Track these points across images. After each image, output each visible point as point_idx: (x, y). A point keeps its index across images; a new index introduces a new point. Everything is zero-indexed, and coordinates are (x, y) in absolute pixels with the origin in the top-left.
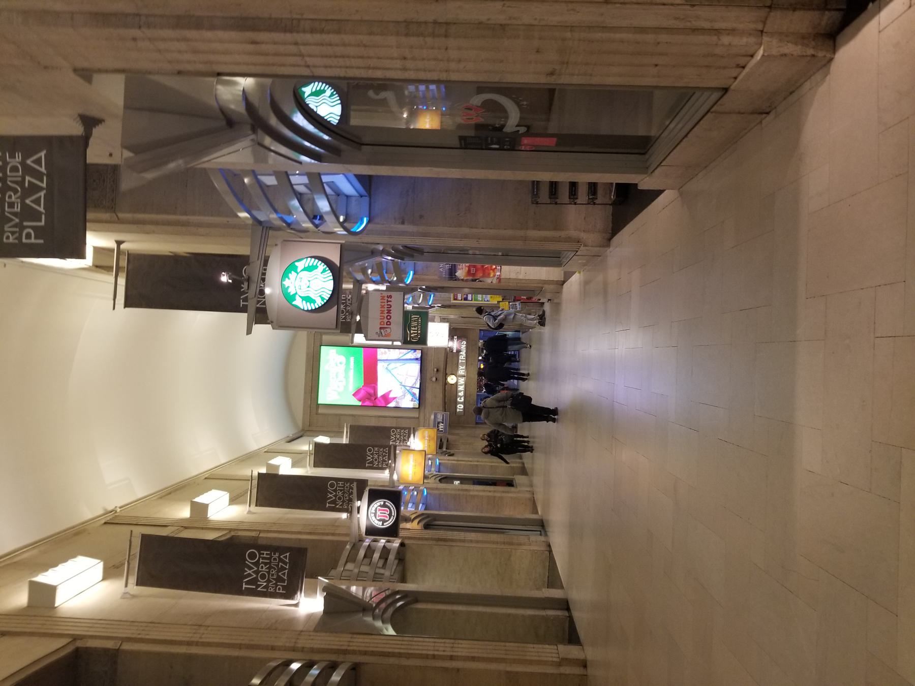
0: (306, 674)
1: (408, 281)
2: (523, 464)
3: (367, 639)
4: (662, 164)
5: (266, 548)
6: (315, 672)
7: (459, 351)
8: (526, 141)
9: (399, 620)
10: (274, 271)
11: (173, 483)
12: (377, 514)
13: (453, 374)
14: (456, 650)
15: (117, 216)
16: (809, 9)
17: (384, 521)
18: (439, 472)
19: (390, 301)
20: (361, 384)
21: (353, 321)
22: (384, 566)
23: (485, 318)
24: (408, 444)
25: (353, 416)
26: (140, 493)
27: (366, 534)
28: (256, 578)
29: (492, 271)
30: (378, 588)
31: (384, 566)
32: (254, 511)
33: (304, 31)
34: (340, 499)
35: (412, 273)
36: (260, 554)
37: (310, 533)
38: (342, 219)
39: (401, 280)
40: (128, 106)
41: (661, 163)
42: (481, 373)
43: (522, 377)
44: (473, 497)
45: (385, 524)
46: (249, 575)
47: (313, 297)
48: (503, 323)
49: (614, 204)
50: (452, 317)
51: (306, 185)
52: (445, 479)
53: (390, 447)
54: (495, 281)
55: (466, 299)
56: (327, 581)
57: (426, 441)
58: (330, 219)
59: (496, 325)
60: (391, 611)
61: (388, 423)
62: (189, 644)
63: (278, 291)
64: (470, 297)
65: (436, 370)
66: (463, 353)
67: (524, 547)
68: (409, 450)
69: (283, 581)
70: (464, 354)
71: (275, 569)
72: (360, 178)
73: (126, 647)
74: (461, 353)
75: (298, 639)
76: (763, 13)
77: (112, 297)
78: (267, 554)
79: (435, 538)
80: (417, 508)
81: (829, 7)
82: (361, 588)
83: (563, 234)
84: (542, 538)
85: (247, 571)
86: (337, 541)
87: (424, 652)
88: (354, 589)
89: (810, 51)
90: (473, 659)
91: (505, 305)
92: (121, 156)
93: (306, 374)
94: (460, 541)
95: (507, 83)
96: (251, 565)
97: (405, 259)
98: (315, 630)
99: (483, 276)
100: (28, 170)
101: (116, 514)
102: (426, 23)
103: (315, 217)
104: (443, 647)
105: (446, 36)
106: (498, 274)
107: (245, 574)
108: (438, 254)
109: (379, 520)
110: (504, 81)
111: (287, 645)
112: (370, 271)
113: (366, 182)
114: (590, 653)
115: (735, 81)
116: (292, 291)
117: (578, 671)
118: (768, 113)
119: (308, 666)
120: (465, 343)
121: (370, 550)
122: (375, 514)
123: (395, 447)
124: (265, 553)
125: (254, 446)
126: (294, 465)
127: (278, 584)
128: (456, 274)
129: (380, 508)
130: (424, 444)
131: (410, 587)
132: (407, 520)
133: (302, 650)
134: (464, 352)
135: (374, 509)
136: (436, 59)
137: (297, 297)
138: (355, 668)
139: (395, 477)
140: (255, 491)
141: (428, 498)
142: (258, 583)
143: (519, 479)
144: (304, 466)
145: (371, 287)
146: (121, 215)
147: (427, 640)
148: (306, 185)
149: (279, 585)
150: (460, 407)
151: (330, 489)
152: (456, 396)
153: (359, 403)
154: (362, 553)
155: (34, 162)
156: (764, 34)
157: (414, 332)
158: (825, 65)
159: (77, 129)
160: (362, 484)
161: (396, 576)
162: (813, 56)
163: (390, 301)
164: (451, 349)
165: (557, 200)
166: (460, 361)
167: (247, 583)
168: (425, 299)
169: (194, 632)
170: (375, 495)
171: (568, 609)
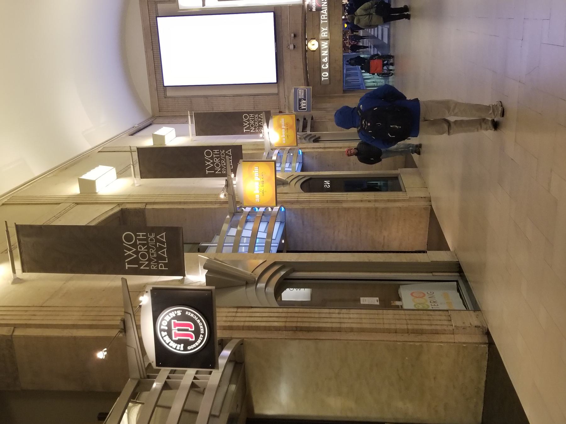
7: (319, 9)
12: (173, 332)
13: (314, 39)
25: (206, 97)
27: (158, 365)
28: (137, 257)
37: (91, 327)
44: (348, 210)
45: (189, 348)
46: (209, 165)
57: (283, 130)
65: (293, 35)
66: (325, 12)
67: (443, 338)
70: (326, 13)
71: (154, 249)
78: (143, 235)
85: (244, 124)
93: (146, 52)
96: (128, 246)
107: (125, 255)
109: (178, 342)
129: (176, 321)
130: (281, 134)
134: (326, 10)
135: (165, 323)
141: (287, 214)
142: (140, 262)
149: (161, 263)
150: (325, 75)
151: (126, 244)
152: (320, 63)
166: (322, 22)
167: (129, 263)
169: (82, 314)
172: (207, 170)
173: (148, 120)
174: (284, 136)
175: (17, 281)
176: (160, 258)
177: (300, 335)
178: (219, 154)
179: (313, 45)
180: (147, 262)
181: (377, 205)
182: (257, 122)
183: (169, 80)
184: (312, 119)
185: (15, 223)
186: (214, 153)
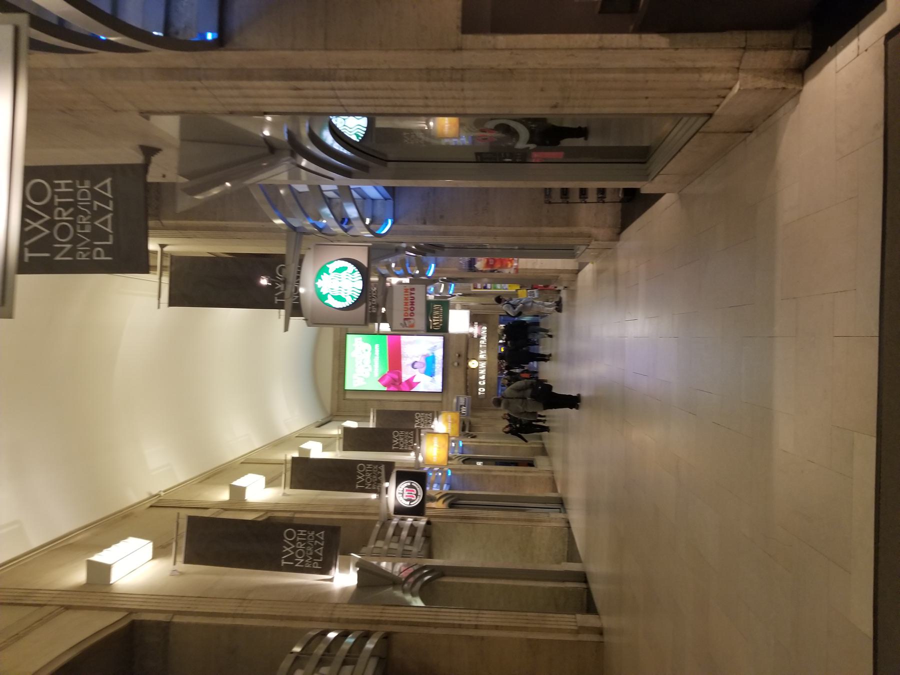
0: (342, 642)
1: (430, 274)
2: (543, 444)
3: (398, 610)
4: (661, 173)
6: (350, 640)
7: (479, 336)
8: (535, 155)
9: (427, 592)
10: (308, 272)
14: (480, 619)
15: (162, 223)
16: (779, 49)
17: (411, 501)
18: (462, 454)
19: (413, 294)
20: (386, 370)
21: (379, 314)
22: (412, 543)
23: (504, 307)
24: (432, 427)
26: (181, 478)
27: (395, 514)
29: (509, 262)
30: (406, 563)
31: (412, 543)
32: (288, 493)
33: (340, 79)
35: (433, 265)
38: (368, 221)
39: (423, 273)
40: (184, 139)
41: (659, 172)
42: (501, 356)
43: (544, 358)
44: (495, 476)
45: (411, 503)
46: (288, 552)
47: (343, 295)
48: (522, 311)
49: (622, 201)
50: (472, 304)
51: (334, 191)
52: (467, 460)
53: (414, 430)
54: (512, 271)
55: (485, 288)
56: (359, 557)
58: (358, 224)
59: (516, 313)
60: (419, 584)
61: (412, 407)
62: (234, 616)
63: (311, 290)
64: (489, 286)
65: (457, 355)
66: (484, 338)
68: (433, 433)
72: (387, 188)
73: (177, 619)
74: (482, 338)
75: (334, 611)
76: (738, 53)
77: (156, 294)
79: (460, 516)
80: (441, 488)
81: (796, 47)
82: (390, 564)
83: (575, 230)
84: (562, 515)
85: (284, 549)
86: (368, 520)
87: (451, 622)
88: (384, 564)
89: (781, 85)
90: (497, 628)
91: (523, 294)
92: (173, 176)
94: (483, 518)
95: (516, 114)
97: (427, 255)
98: (349, 603)
99: (502, 267)
100: (97, 196)
101: (160, 498)
102: (444, 69)
103: (343, 220)
104: (467, 617)
105: (462, 80)
106: (515, 264)
107: (284, 551)
108: (458, 250)
109: (407, 500)
110: (514, 113)
111: (325, 616)
112: (393, 265)
113: (391, 190)
114: (605, 621)
115: (717, 108)
116: (324, 291)
117: (595, 638)
118: (751, 132)
119: (344, 635)
120: (486, 328)
121: (398, 529)
122: (403, 494)
123: (420, 430)
124: (302, 532)
125: (285, 431)
126: (325, 448)
128: (476, 266)
129: (407, 488)
131: (436, 562)
132: (433, 499)
133: (338, 620)
136: (454, 98)
137: (329, 297)
138: (387, 637)
139: (421, 459)
140: (289, 474)
143: (541, 461)
144: (333, 450)
145: (394, 280)
147: (453, 610)
148: (334, 191)
150: (482, 391)
151: (359, 471)
152: (478, 380)
153: (385, 389)
154: (391, 531)
156: (740, 70)
157: (436, 321)
158: (795, 96)
159: (138, 158)
160: (389, 466)
161: (423, 553)
162: (784, 88)
163: (413, 294)
164: (472, 335)
165: (568, 200)
167: (286, 560)
168: (447, 289)
170: (402, 476)
171: (586, 581)
173: (328, 417)
174: (450, 428)
176: (315, 556)
177: (464, 521)
179: (473, 364)
181: (516, 474)
183: (348, 386)
184: (470, 423)
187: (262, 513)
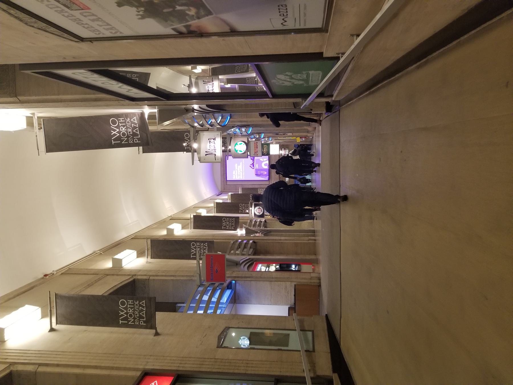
5: (198, 241)
11: (112, 243)
34: (131, 316)
36: (196, 244)
46: (224, 225)
47: (242, 150)
69: (143, 318)
85: (121, 313)
109: (258, 213)
116: (237, 149)
117: (314, 242)
121: (256, 222)
122: (257, 211)
126: (207, 213)
127: (140, 320)
146: (21, 98)
149: (141, 320)
151: (240, 206)
155: (133, 120)
172: (120, 320)
173: (220, 192)
175: (52, 330)
178: (133, 305)
180: (133, 320)
182: (137, 311)
185: (55, 293)
186: (128, 303)
187: (129, 277)
